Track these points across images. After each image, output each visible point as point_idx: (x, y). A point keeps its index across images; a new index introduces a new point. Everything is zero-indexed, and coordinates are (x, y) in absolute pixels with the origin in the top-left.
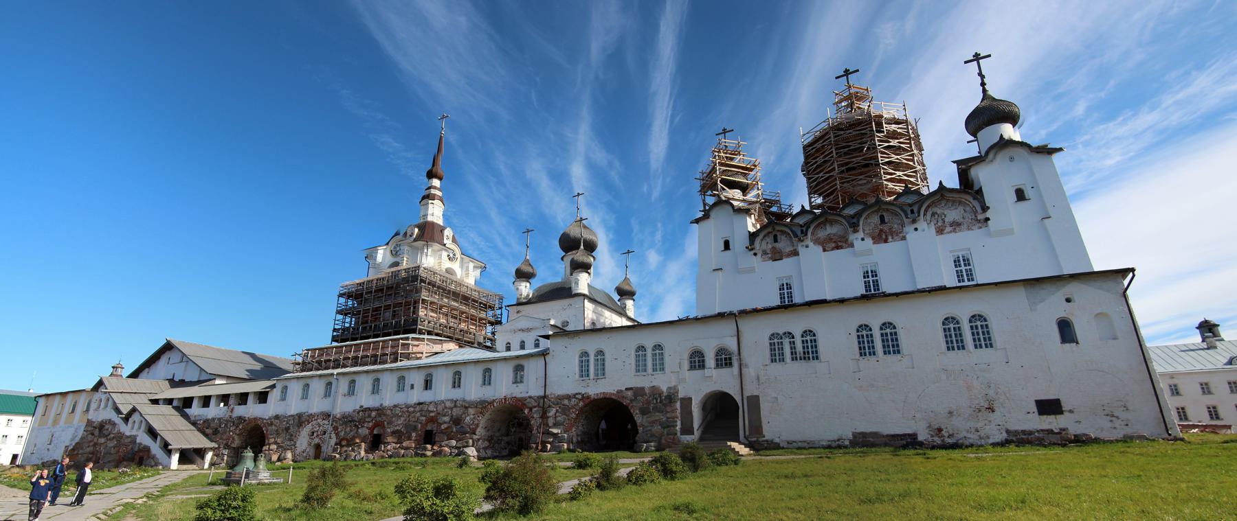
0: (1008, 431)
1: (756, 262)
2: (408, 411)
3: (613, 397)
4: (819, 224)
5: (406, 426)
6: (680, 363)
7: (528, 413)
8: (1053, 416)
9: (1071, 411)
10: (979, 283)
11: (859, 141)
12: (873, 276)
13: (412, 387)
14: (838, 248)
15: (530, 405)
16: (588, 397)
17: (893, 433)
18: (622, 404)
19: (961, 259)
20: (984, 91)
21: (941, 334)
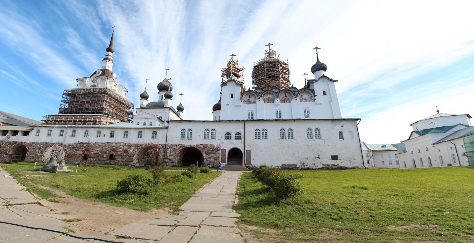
0: (323, 165)
1: (242, 104)
2: (102, 145)
3: (195, 147)
5: (101, 152)
6: (222, 136)
7: (158, 150)
8: (335, 161)
9: (340, 159)
10: (311, 119)
11: (274, 68)
12: (279, 113)
13: (105, 135)
14: (269, 102)
15: (160, 148)
16: (184, 146)
17: (289, 164)
19: (306, 111)
20: (318, 59)
21: (306, 134)
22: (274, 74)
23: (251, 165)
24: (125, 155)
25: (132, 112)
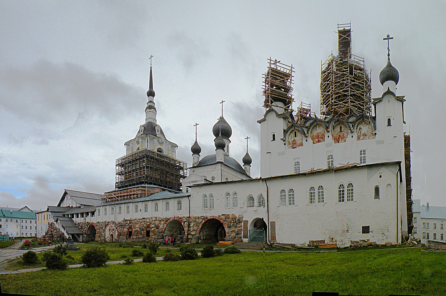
2: (139, 222)
4: (313, 128)
9: (372, 232)
18: (220, 222)
22: (342, 90)
23: (276, 242)
24: (156, 231)
25: (186, 174)
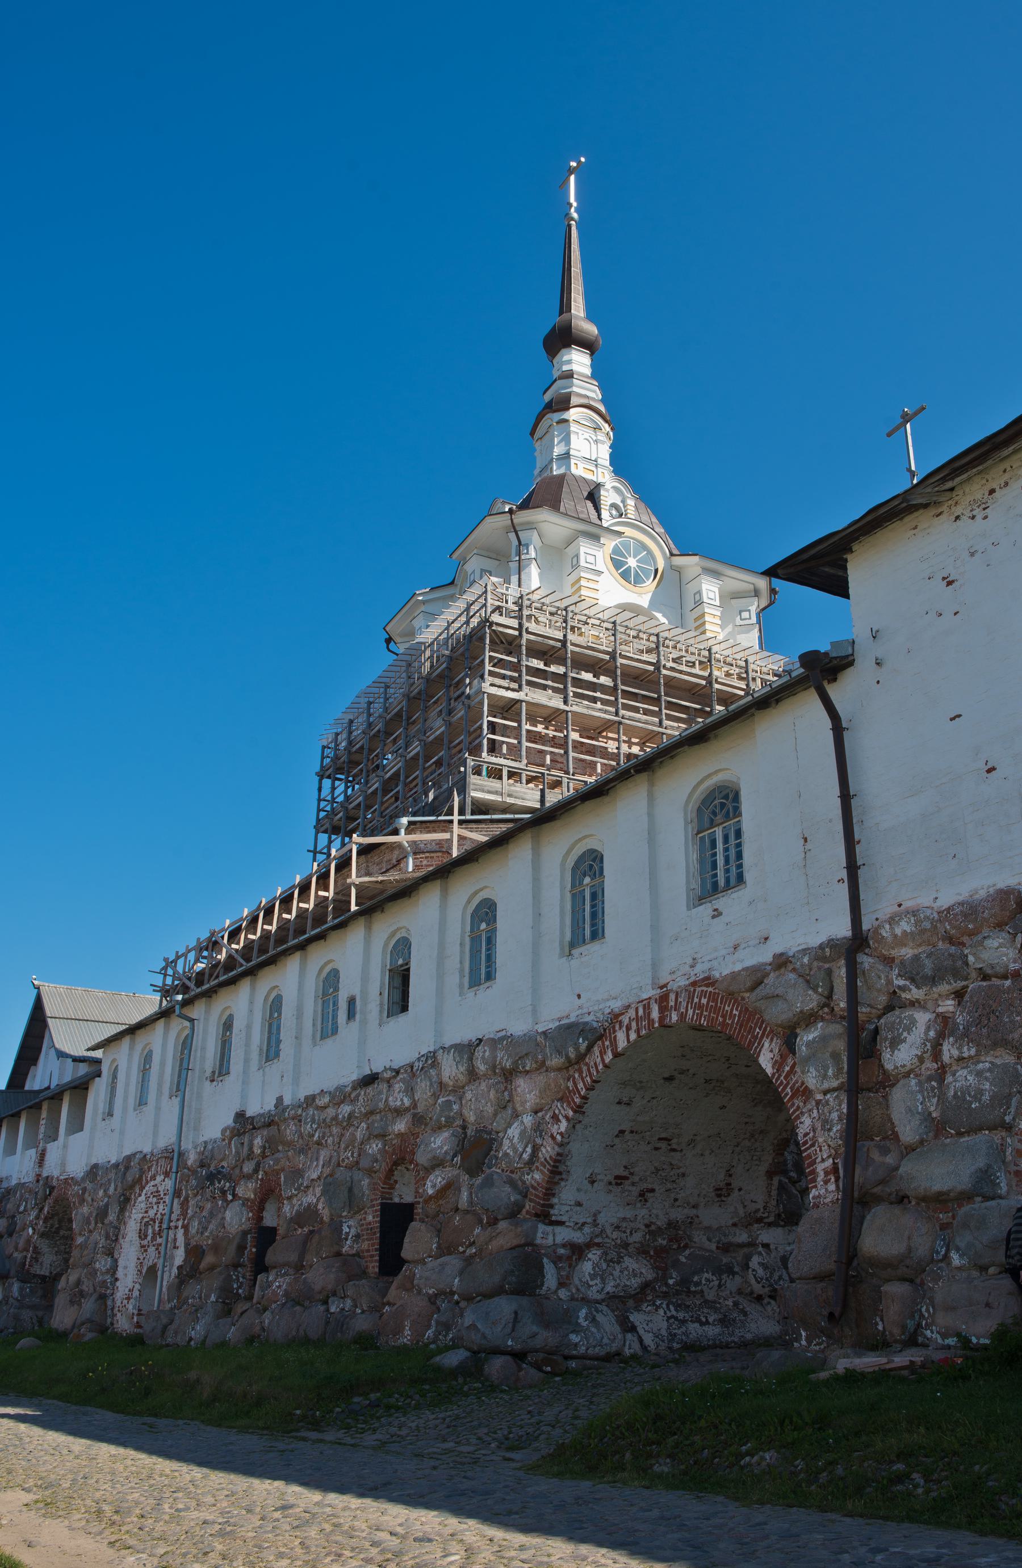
7: (779, 1065)
